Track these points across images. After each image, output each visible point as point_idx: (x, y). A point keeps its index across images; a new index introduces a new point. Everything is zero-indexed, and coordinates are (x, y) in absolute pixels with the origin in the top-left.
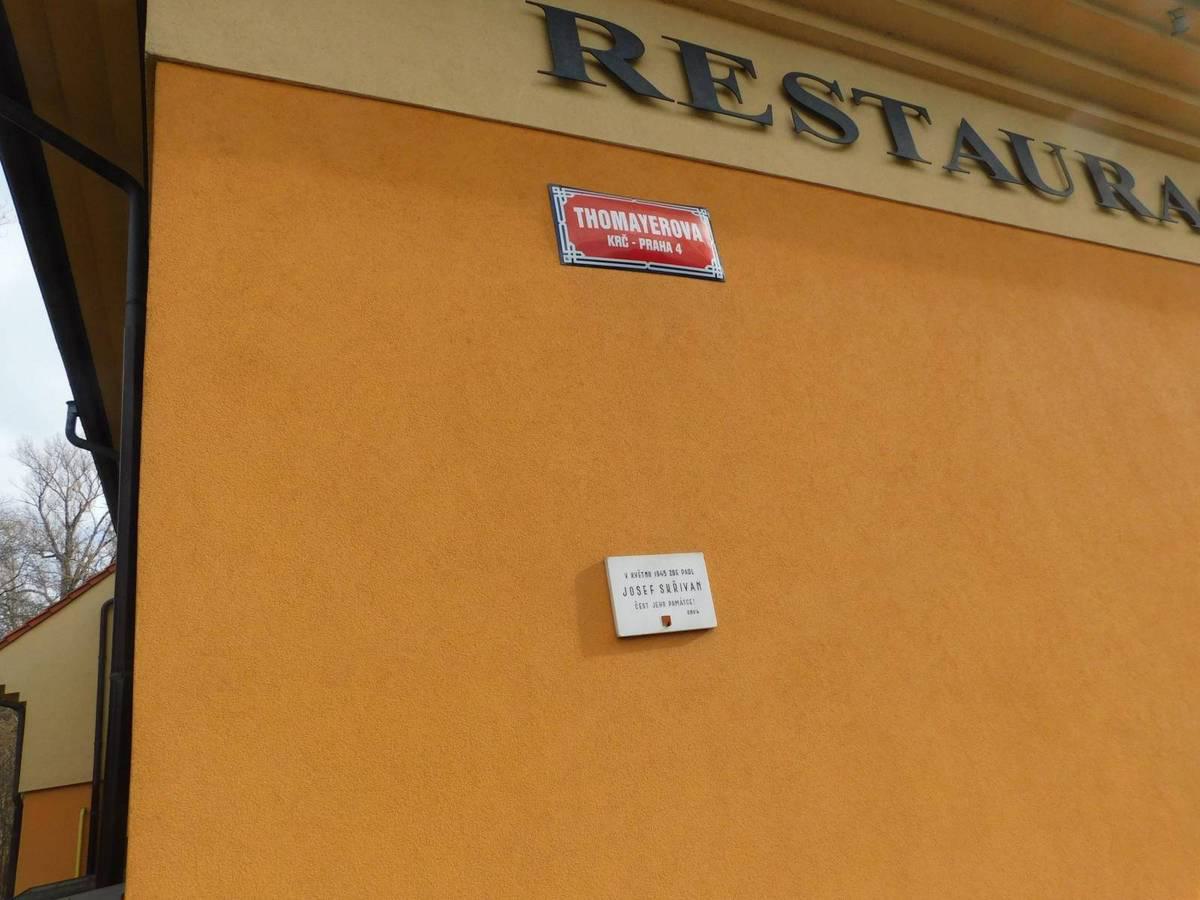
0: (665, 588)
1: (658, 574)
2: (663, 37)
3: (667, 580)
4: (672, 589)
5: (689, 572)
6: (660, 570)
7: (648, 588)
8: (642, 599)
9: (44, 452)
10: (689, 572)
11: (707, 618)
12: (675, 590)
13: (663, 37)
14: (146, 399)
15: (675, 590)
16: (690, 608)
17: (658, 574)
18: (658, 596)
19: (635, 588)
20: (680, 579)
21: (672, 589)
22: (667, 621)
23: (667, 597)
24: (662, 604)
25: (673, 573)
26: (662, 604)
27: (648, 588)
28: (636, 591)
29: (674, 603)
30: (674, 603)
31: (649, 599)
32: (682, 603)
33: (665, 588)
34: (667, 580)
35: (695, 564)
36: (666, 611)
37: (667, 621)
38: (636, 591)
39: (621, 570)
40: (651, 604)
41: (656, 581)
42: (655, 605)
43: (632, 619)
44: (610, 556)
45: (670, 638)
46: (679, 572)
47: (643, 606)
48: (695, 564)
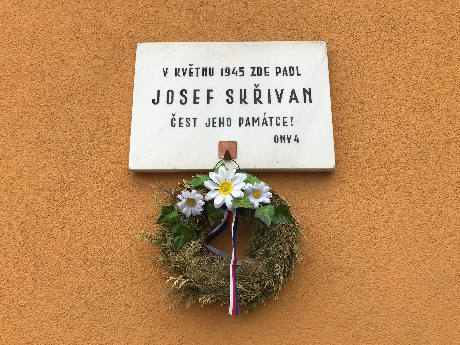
0: (236, 96)
1: (227, 72)
3: (236, 83)
4: (250, 98)
5: (292, 71)
6: (234, 64)
7: (202, 95)
8: (189, 110)
9: (268, 217)
10: (292, 71)
12: (257, 100)
15: (257, 100)
16: (281, 131)
17: (227, 72)
18: (220, 108)
19: (184, 125)
21: (250, 98)
23: (237, 111)
24: (226, 122)
26: (226, 122)
27: (202, 95)
31: (202, 112)
33: (236, 96)
40: (202, 122)
41: (220, 84)
42: (211, 123)
46: (272, 71)
48: (310, 60)
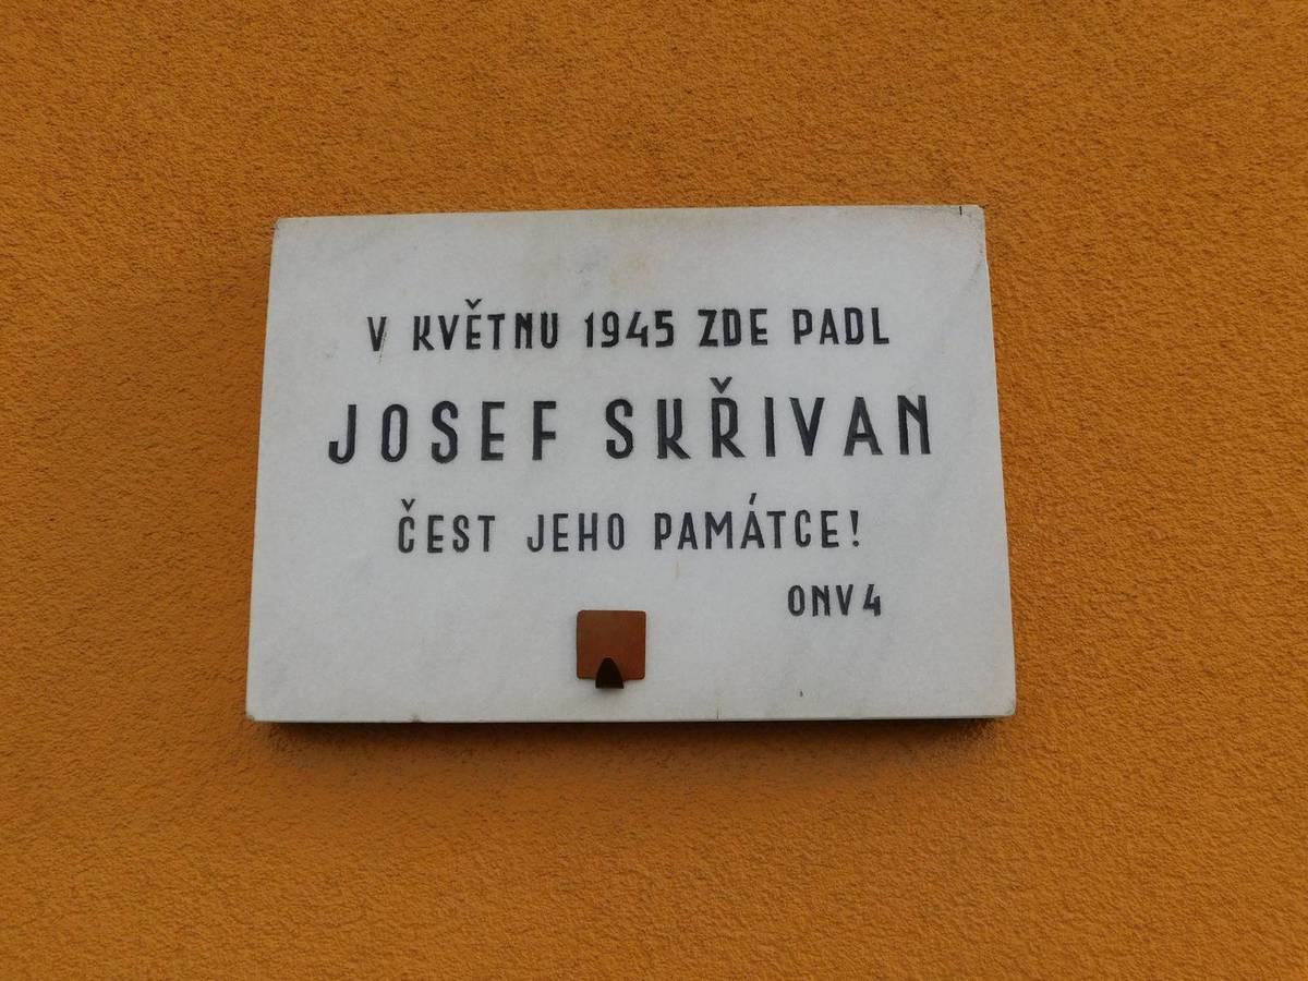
1: (608, 330)
2: (352, 410)
4: (696, 434)
5: (855, 327)
7: (514, 425)
8: (462, 487)
10: (855, 327)
11: (946, 645)
12: (723, 441)
13: (352, 410)
15: (723, 441)
16: (814, 567)
17: (608, 330)
18: (581, 476)
19: (447, 544)
20: (770, 372)
21: (696, 434)
22: (611, 647)
23: (647, 486)
25: (729, 327)
27: (514, 425)
29: (681, 531)
30: (681, 531)
31: (511, 490)
33: (644, 426)
35: (920, 280)
36: (609, 581)
37: (611, 647)
39: (341, 298)
40: (513, 530)
41: (579, 378)
42: (549, 535)
44: (999, 253)
45: (620, 750)
46: (778, 325)
47: (462, 533)
48: (920, 280)
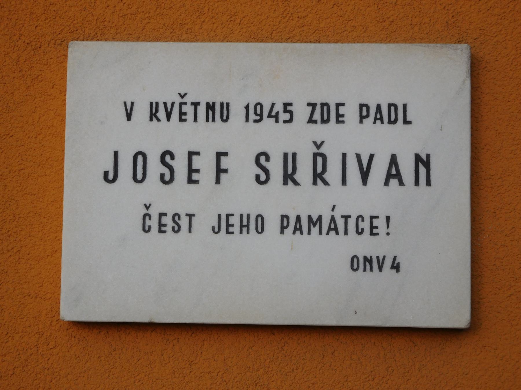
0: (276, 167)
1: (257, 113)
2: (116, 154)
4: (305, 173)
5: (393, 114)
7: (205, 164)
8: (177, 198)
10: (393, 114)
12: (318, 177)
13: (116, 154)
14: (156, 320)
15: (318, 177)
16: (366, 246)
17: (257, 113)
21: (305, 173)
25: (324, 113)
27: (205, 164)
28: (155, 168)
32: (333, 228)
33: (276, 167)
34: (298, 138)
35: (430, 86)
38: (155, 168)
40: (204, 222)
41: (241, 139)
43: (374, 232)
46: (351, 112)
47: (178, 223)
48: (430, 86)
